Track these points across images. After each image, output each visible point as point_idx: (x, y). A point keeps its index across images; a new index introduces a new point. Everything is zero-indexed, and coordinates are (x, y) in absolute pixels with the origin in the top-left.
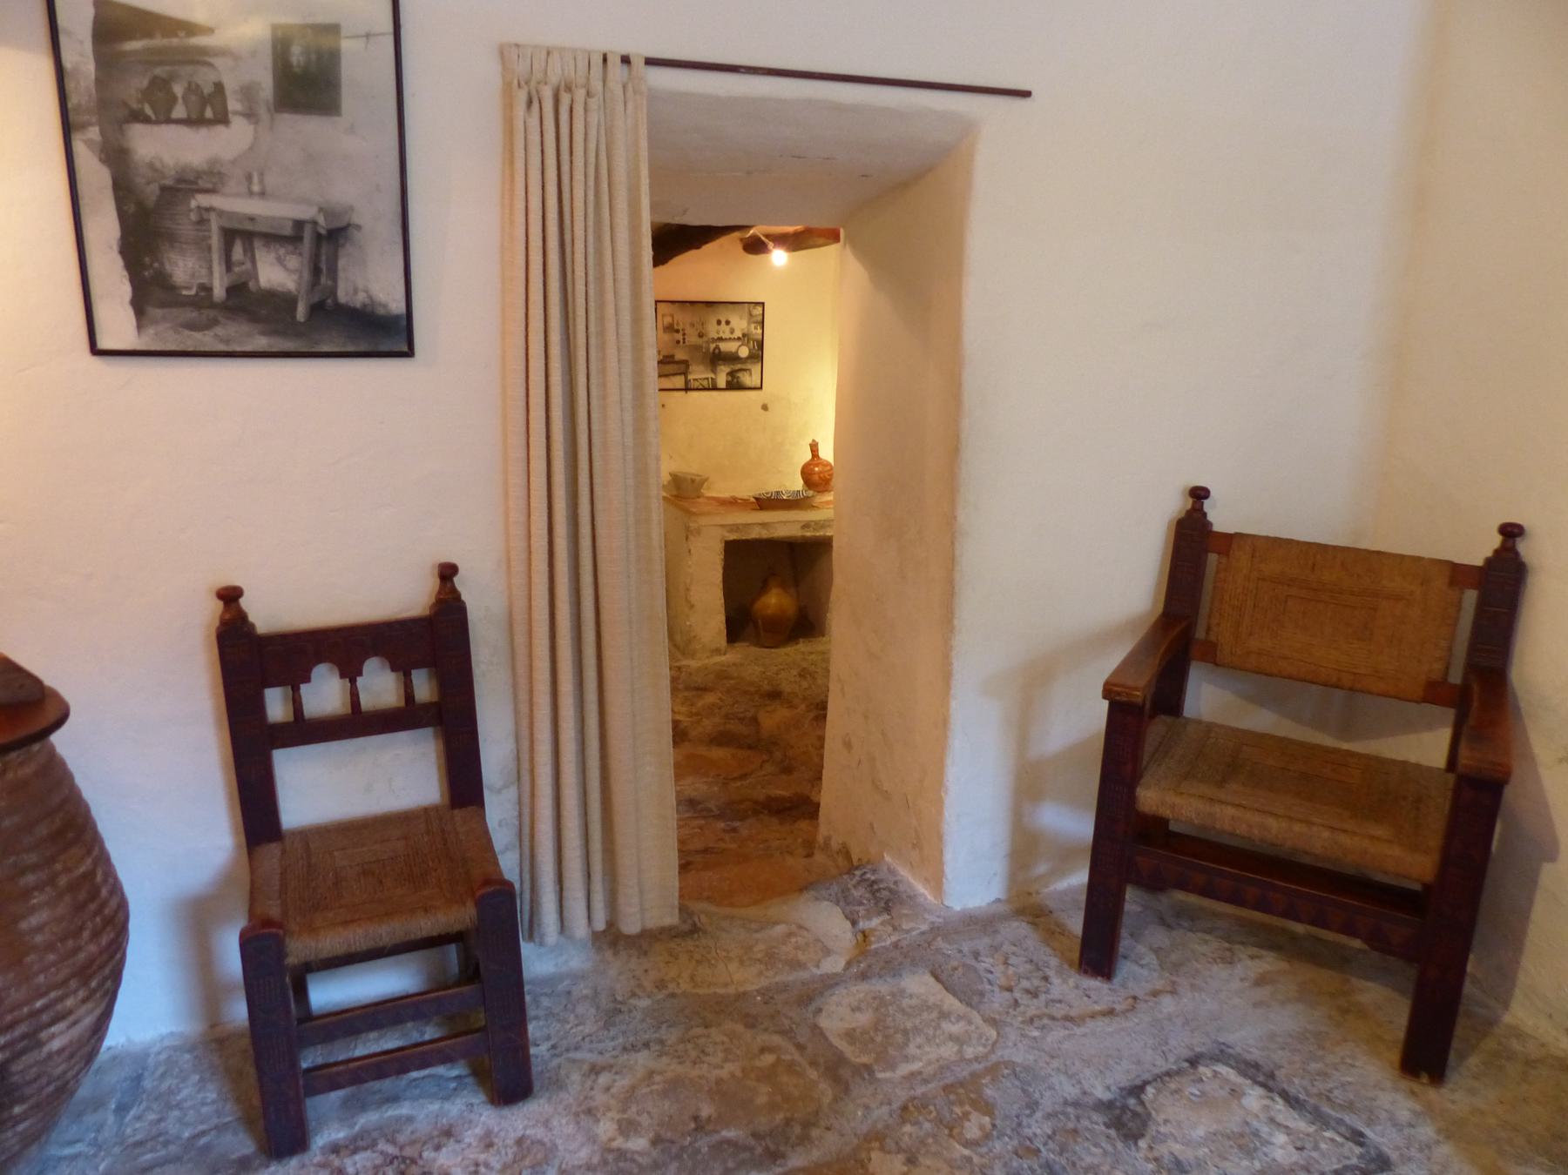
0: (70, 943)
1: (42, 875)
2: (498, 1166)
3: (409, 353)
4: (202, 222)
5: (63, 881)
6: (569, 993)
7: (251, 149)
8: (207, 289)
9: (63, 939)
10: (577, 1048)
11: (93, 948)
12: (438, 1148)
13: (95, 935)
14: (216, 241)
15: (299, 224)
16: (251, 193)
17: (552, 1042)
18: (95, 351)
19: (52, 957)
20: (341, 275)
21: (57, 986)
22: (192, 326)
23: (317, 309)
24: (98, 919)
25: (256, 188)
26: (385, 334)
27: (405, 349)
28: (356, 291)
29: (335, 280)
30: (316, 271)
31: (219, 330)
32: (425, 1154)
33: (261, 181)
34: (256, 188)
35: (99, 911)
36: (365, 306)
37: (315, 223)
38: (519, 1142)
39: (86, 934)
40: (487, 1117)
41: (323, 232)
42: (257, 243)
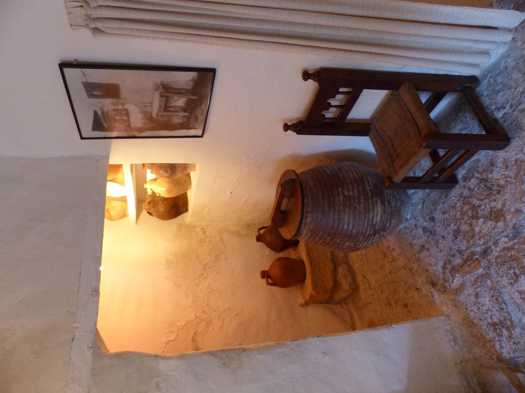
0: (357, 212)
1: (337, 213)
2: (513, 175)
3: (213, 71)
4: (162, 116)
5: (341, 208)
6: (506, 68)
7: (135, 105)
8: (184, 117)
9: (355, 214)
10: (520, 104)
11: (362, 206)
12: (491, 172)
13: (360, 204)
14: (168, 114)
15: (161, 96)
16: (151, 106)
17: (510, 103)
18: (202, 136)
19: (357, 218)
20: (181, 87)
21: (365, 219)
22: (197, 119)
23: (193, 94)
24: (356, 201)
25: (149, 105)
26: (206, 76)
27: (212, 74)
28: (187, 84)
29: (183, 89)
30: (179, 93)
31: (198, 115)
32: (489, 176)
33: (147, 103)
34: (149, 105)
35: (354, 198)
36: (193, 82)
37: (161, 93)
38: (516, 161)
39: (358, 207)
40: (501, 154)
41: (164, 91)
42: (169, 105)
